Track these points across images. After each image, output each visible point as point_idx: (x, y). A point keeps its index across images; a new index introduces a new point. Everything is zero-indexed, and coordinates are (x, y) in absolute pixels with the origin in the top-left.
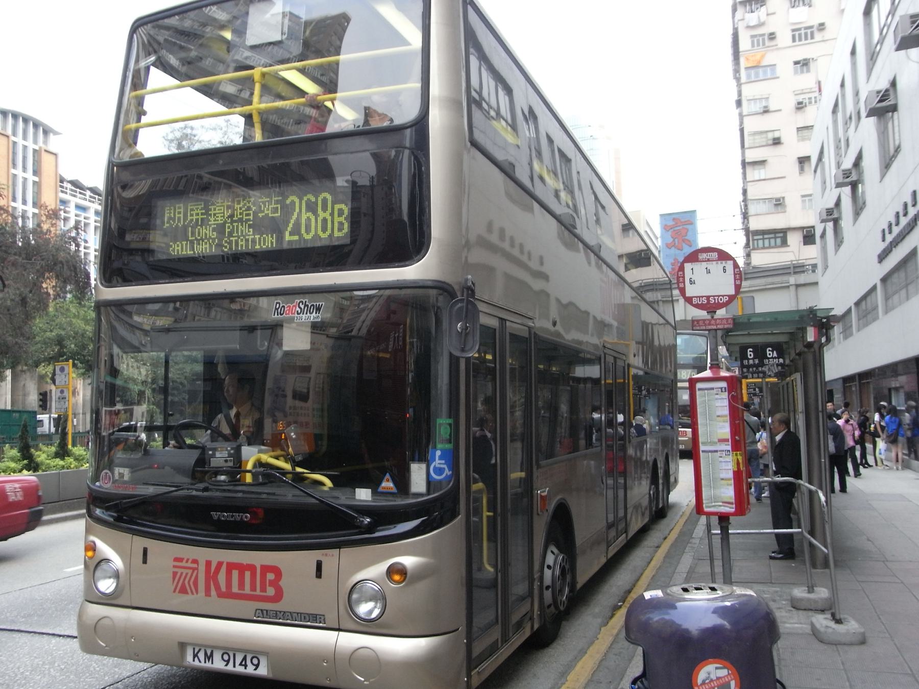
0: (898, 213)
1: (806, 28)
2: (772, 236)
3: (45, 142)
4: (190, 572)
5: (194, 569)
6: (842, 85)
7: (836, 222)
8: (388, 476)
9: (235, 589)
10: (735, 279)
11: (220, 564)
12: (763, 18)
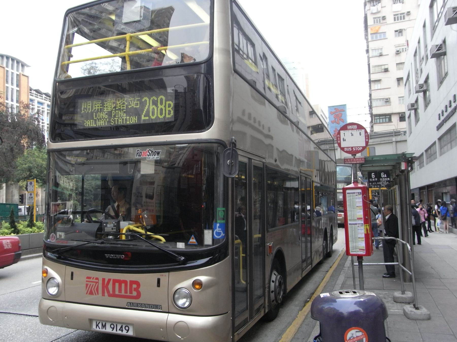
0: (446, 106)
1: (401, 14)
2: (384, 117)
3: (22, 71)
4: (94, 284)
5: (96, 283)
6: (419, 42)
7: (416, 110)
8: (193, 236)
9: (117, 292)
10: (366, 139)
11: (109, 280)
12: (380, 9)
